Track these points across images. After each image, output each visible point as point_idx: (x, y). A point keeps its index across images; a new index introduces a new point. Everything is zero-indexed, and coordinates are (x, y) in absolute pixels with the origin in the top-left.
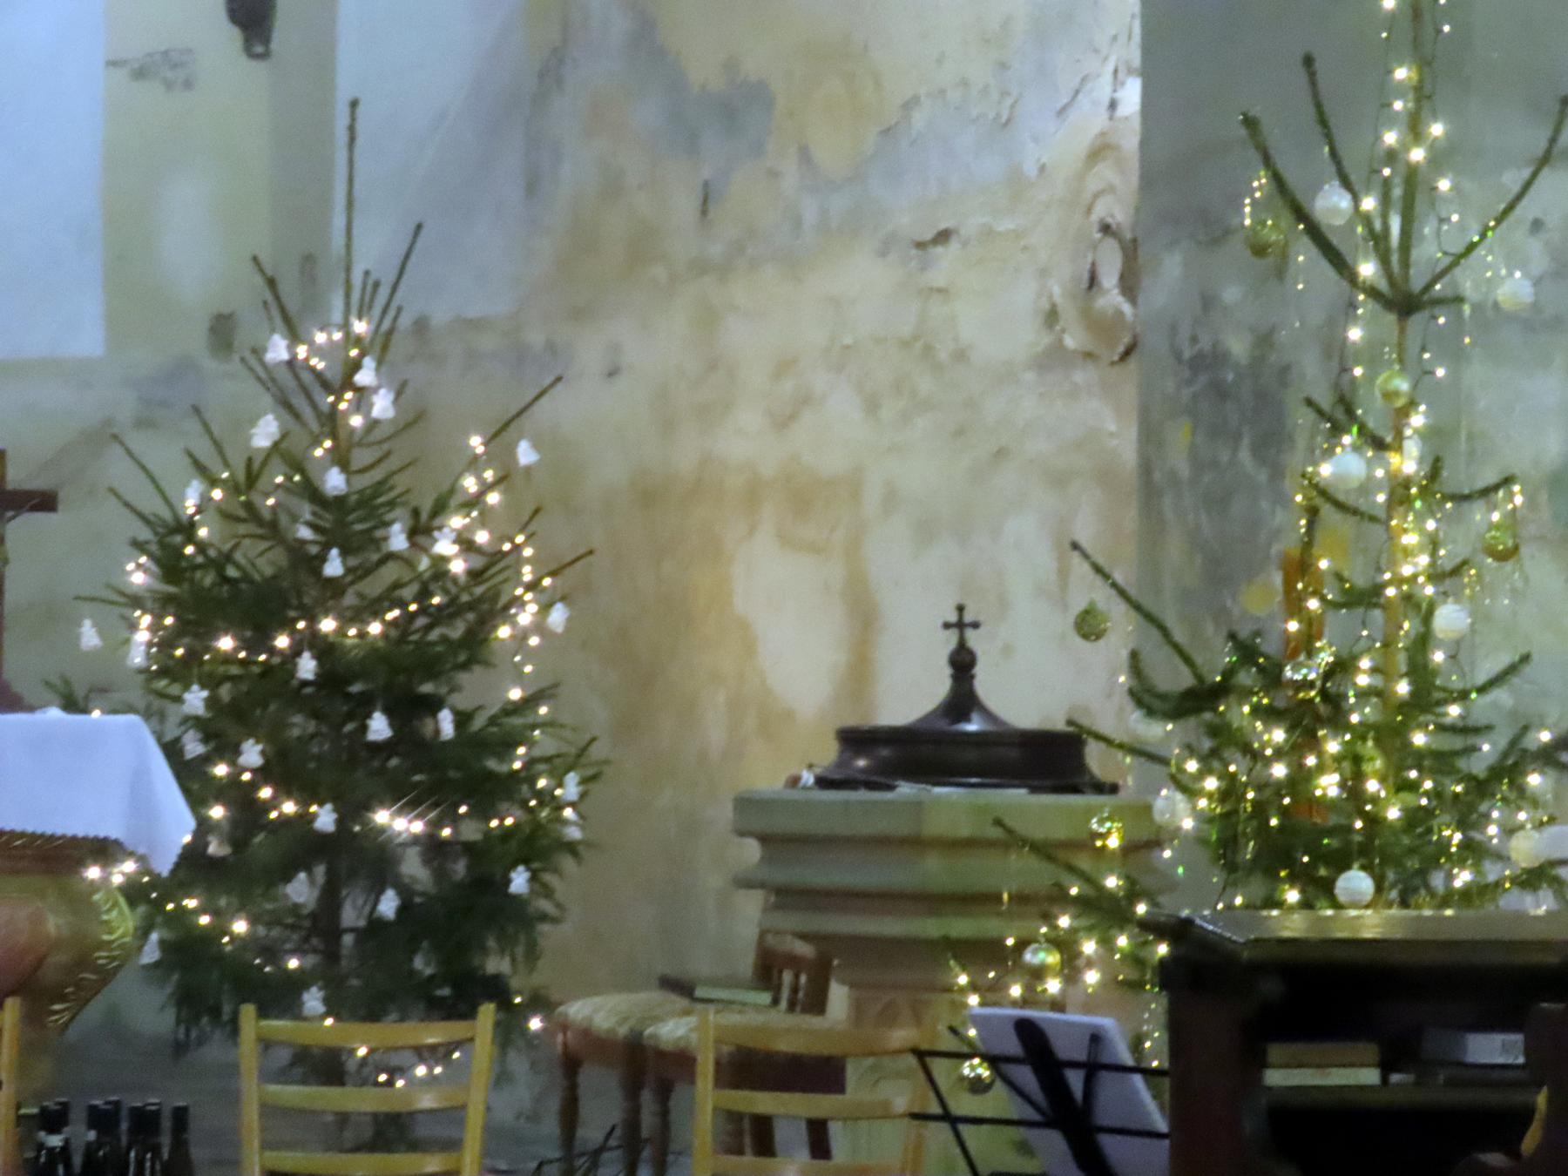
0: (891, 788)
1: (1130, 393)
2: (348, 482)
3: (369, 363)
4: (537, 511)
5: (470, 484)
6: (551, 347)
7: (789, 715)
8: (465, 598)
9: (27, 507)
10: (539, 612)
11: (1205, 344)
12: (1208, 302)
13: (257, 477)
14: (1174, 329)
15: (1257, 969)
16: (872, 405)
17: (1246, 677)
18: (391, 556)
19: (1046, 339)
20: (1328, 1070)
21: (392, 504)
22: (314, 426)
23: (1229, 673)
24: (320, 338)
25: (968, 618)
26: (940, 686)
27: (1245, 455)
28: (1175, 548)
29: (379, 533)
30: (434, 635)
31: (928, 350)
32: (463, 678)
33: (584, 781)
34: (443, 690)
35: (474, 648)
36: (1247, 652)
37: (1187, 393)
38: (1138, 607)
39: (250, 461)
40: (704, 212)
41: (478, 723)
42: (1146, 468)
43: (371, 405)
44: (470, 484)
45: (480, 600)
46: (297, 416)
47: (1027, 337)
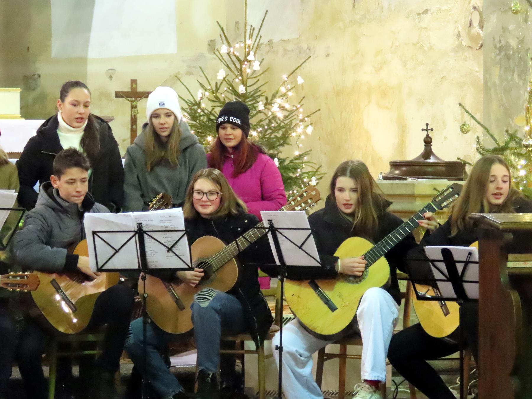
0: (406, 179)
1: (482, 59)
2: (246, 89)
3: (252, 53)
4: (304, 97)
5: (283, 90)
6: (309, 48)
7: (381, 159)
8: (282, 124)
9: (144, 97)
10: (304, 128)
11: (503, 43)
12: (504, 30)
13: (219, 89)
14: (494, 39)
15: (505, 231)
16: (405, 64)
17: (512, 144)
18: (260, 112)
19: (457, 43)
20: (527, 262)
21: (259, 96)
22: (236, 73)
23: (507, 143)
24: (237, 46)
25: (429, 128)
26: (421, 148)
27: (516, 77)
28: (495, 106)
29: (255, 105)
30: (272, 136)
31: (422, 46)
32: (281, 148)
33: (318, 179)
34: (276, 152)
35: (285, 140)
36: (513, 137)
37: (498, 57)
38: (482, 126)
39: (216, 84)
40: (354, 6)
41: (287, 162)
42: (486, 82)
43: (253, 66)
44: (283, 90)
45: (287, 125)
46: (231, 70)
47: (451, 42)
